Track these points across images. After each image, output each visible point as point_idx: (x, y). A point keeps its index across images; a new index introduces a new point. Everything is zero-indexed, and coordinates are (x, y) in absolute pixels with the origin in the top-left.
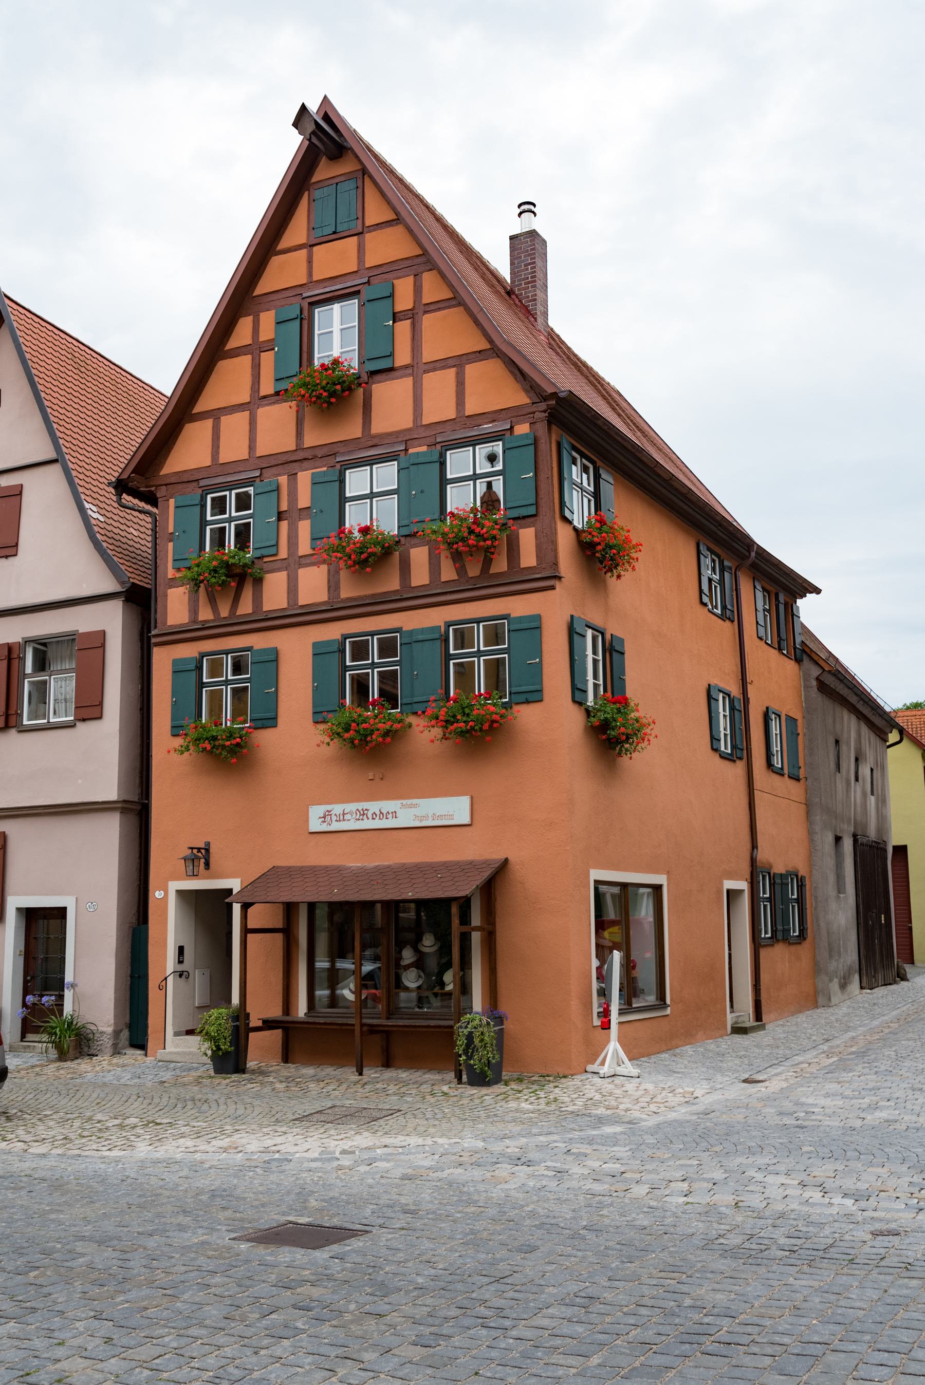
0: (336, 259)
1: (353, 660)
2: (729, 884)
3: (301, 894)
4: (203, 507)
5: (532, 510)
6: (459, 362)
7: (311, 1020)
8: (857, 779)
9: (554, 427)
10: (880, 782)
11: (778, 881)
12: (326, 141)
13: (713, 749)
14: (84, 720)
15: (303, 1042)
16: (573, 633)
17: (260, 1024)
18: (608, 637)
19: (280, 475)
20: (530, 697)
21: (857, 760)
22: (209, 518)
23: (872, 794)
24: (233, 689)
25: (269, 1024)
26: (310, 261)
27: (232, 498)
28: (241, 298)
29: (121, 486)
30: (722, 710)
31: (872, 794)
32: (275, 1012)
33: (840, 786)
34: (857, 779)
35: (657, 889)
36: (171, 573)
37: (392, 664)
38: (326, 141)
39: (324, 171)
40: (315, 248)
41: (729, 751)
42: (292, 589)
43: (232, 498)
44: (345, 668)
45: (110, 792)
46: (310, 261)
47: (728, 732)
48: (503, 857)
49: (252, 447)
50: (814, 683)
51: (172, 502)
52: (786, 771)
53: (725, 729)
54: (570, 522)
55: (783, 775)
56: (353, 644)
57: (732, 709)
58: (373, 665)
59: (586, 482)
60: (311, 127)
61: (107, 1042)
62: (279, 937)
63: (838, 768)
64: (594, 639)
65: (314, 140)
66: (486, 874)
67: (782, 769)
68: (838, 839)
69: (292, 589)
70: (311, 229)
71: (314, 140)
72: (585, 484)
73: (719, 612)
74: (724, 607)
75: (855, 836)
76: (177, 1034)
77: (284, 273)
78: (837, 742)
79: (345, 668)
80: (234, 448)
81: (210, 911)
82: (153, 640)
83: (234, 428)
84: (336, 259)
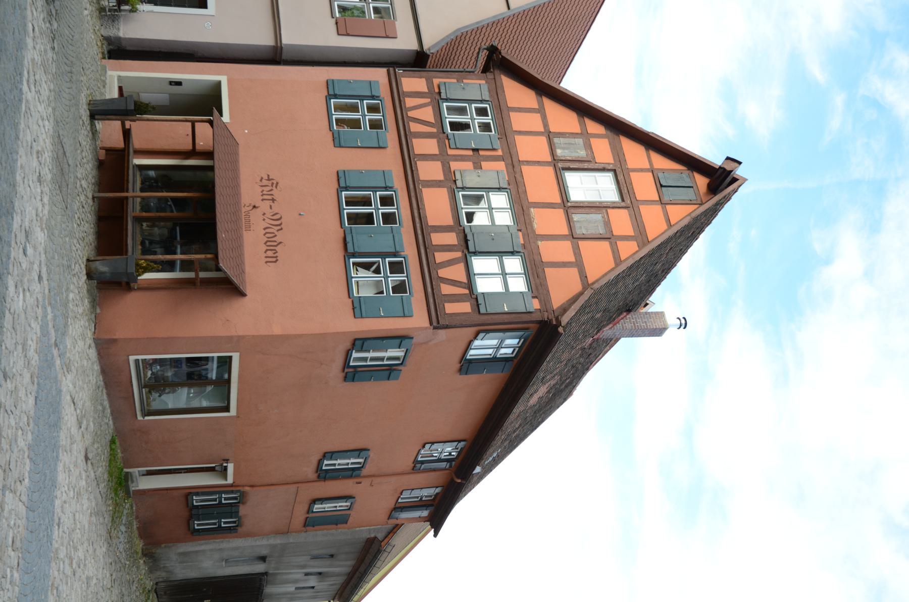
0: (644, 186)
1: (390, 263)
2: (231, 467)
3: (219, 164)
4: (482, 101)
5: (483, 310)
6: (579, 263)
7: (131, 167)
8: (307, 574)
9: (537, 326)
10: (305, 595)
11: (234, 509)
12: (720, 180)
13: (325, 453)
14: (337, 23)
15: (112, 167)
16: (400, 339)
17: (127, 127)
18: (400, 368)
19: (503, 150)
20: (357, 311)
21: (320, 574)
22: (473, 105)
23: (296, 588)
24: (372, 213)
25: (127, 134)
26: (642, 170)
27: (488, 120)
28: (617, 127)
29: (493, 50)
30: (351, 462)
31: (296, 588)
32: (137, 142)
33: (302, 560)
34: (307, 574)
35: (227, 409)
36: (436, 81)
37: (378, 220)
38: (720, 180)
39: (702, 182)
40: (651, 174)
41: (324, 468)
42: (426, 157)
43: (488, 120)
44: (362, 100)
45: (288, 39)
46: (642, 170)
47: (337, 467)
48: (248, 292)
49: (528, 163)
50: (373, 536)
51: (483, 82)
52: (310, 515)
53: (339, 464)
54: (475, 338)
55: (308, 513)
56: (401, 263)
57: (353, 469)
58: (377, 209)
59: (506, 352)
60: (728, 168)
61: (111, 32)
62: (190, 147)
63: (315, 558)
64: (397, 358)
65: (719, 173)
66: (235, 280)
67: (313, 512)
68: (263, 559)
69: (426, 157)
70: (663, 171)
71: (719, 173)
72: (503, 351)
73: (419, 459)
74: (422, 462)
75: (266, 574)
76: (120, 78)
77: (635, 153)
78: (332, 556)
79: (362, 100)
80: (518, 121)
81: (206, 103)
82: (391, 69)
83: (533, 122)
84: (644, 186)
